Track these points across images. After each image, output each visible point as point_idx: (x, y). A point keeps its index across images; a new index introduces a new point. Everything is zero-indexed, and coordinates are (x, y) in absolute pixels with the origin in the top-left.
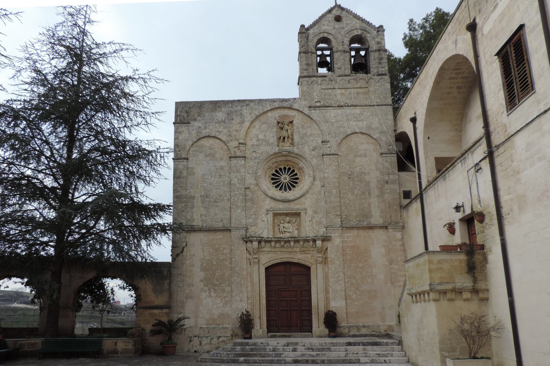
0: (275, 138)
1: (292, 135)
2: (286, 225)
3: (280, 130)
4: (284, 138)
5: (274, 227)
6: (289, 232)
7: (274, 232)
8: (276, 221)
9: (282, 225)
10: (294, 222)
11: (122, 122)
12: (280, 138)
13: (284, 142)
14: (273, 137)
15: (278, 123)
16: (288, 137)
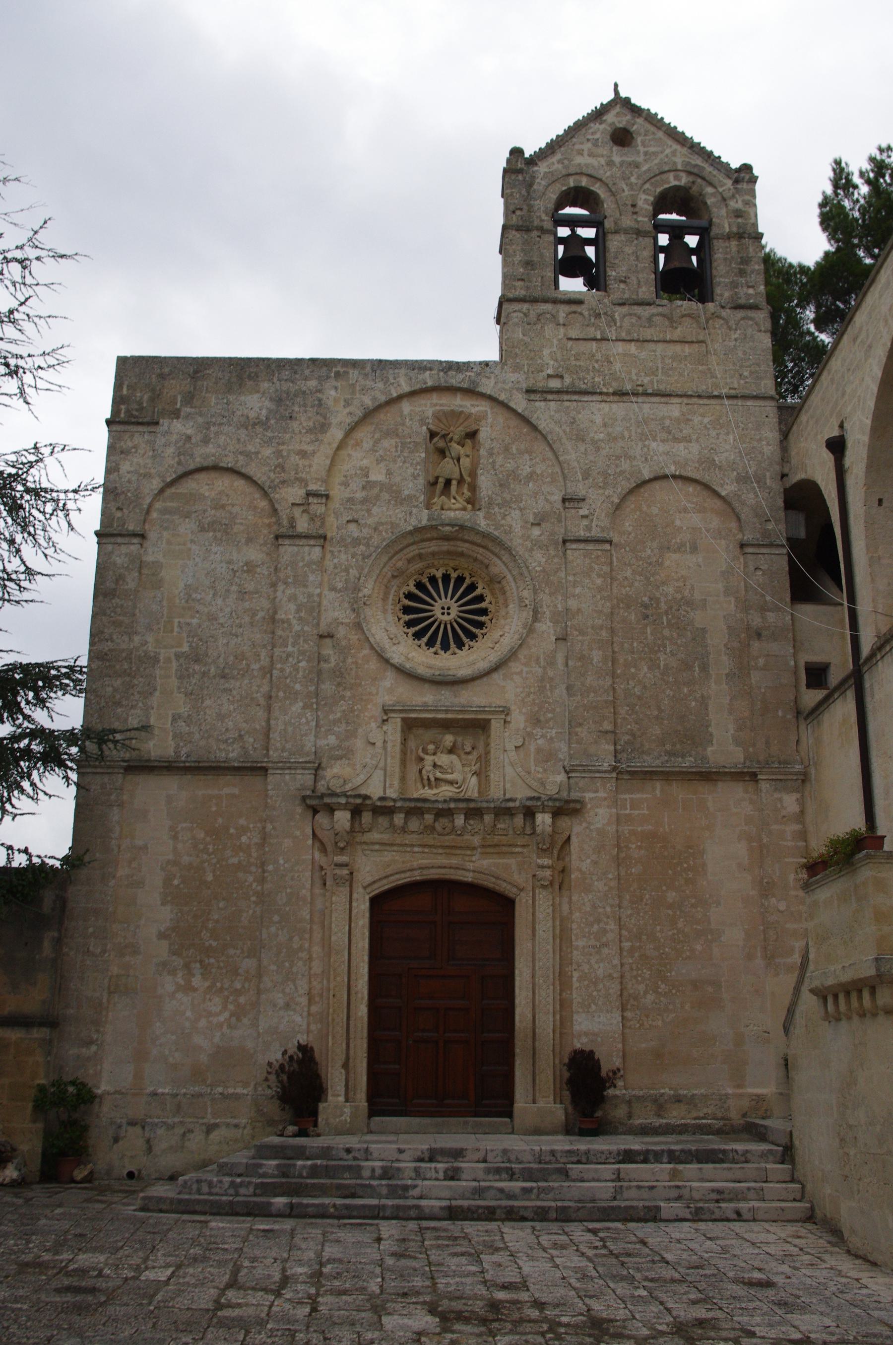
0: (421, 481)
1: (473, 474)
2: (443, 759)
4: (448, 482)
5: (403, 763)
6: (451, 783)
7: (403, 779)
8: (412, 744)
9: (429, 759)
10: (468, 749)
12: (435, 483)
14: (415, 477)
15: (432, 435)
16: (461, 481)
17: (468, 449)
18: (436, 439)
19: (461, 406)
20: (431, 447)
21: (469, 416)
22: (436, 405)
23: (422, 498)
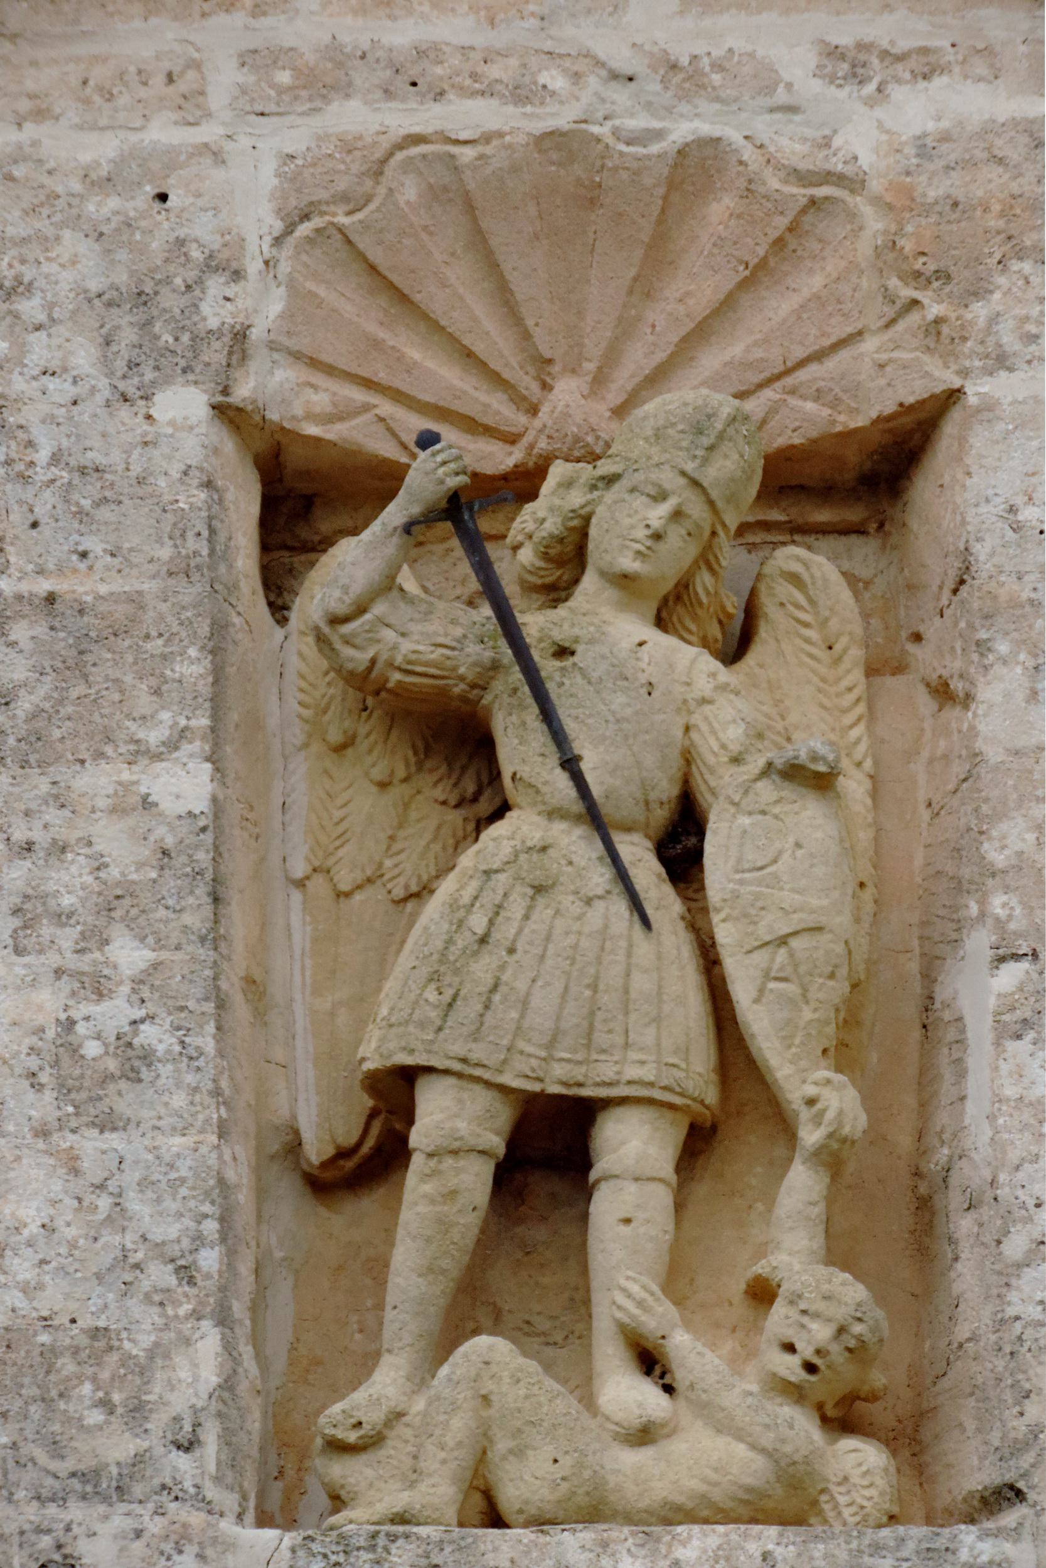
0: (175, 1151)
1: (896, 1024)
3: (370, 807)
4: (549, 1147)
11: (567, 958)
12: (372, 1162)
13: (559, 1329)
14: (86, 1086)
15: (301, 500)
16: (726, 1124)
17: (803, 683)
18: (349, 563)
19: (684, 77)
20: (287, 665)
21: (820, 198)
22: (322, 80)
23: (198, 1368)
